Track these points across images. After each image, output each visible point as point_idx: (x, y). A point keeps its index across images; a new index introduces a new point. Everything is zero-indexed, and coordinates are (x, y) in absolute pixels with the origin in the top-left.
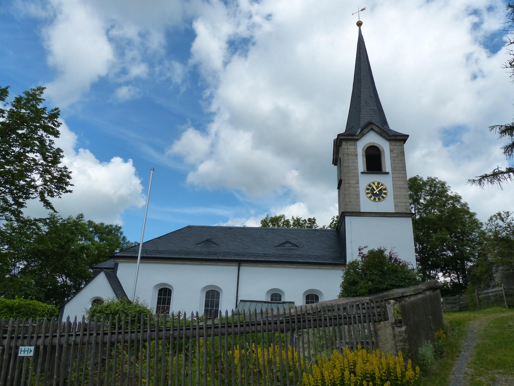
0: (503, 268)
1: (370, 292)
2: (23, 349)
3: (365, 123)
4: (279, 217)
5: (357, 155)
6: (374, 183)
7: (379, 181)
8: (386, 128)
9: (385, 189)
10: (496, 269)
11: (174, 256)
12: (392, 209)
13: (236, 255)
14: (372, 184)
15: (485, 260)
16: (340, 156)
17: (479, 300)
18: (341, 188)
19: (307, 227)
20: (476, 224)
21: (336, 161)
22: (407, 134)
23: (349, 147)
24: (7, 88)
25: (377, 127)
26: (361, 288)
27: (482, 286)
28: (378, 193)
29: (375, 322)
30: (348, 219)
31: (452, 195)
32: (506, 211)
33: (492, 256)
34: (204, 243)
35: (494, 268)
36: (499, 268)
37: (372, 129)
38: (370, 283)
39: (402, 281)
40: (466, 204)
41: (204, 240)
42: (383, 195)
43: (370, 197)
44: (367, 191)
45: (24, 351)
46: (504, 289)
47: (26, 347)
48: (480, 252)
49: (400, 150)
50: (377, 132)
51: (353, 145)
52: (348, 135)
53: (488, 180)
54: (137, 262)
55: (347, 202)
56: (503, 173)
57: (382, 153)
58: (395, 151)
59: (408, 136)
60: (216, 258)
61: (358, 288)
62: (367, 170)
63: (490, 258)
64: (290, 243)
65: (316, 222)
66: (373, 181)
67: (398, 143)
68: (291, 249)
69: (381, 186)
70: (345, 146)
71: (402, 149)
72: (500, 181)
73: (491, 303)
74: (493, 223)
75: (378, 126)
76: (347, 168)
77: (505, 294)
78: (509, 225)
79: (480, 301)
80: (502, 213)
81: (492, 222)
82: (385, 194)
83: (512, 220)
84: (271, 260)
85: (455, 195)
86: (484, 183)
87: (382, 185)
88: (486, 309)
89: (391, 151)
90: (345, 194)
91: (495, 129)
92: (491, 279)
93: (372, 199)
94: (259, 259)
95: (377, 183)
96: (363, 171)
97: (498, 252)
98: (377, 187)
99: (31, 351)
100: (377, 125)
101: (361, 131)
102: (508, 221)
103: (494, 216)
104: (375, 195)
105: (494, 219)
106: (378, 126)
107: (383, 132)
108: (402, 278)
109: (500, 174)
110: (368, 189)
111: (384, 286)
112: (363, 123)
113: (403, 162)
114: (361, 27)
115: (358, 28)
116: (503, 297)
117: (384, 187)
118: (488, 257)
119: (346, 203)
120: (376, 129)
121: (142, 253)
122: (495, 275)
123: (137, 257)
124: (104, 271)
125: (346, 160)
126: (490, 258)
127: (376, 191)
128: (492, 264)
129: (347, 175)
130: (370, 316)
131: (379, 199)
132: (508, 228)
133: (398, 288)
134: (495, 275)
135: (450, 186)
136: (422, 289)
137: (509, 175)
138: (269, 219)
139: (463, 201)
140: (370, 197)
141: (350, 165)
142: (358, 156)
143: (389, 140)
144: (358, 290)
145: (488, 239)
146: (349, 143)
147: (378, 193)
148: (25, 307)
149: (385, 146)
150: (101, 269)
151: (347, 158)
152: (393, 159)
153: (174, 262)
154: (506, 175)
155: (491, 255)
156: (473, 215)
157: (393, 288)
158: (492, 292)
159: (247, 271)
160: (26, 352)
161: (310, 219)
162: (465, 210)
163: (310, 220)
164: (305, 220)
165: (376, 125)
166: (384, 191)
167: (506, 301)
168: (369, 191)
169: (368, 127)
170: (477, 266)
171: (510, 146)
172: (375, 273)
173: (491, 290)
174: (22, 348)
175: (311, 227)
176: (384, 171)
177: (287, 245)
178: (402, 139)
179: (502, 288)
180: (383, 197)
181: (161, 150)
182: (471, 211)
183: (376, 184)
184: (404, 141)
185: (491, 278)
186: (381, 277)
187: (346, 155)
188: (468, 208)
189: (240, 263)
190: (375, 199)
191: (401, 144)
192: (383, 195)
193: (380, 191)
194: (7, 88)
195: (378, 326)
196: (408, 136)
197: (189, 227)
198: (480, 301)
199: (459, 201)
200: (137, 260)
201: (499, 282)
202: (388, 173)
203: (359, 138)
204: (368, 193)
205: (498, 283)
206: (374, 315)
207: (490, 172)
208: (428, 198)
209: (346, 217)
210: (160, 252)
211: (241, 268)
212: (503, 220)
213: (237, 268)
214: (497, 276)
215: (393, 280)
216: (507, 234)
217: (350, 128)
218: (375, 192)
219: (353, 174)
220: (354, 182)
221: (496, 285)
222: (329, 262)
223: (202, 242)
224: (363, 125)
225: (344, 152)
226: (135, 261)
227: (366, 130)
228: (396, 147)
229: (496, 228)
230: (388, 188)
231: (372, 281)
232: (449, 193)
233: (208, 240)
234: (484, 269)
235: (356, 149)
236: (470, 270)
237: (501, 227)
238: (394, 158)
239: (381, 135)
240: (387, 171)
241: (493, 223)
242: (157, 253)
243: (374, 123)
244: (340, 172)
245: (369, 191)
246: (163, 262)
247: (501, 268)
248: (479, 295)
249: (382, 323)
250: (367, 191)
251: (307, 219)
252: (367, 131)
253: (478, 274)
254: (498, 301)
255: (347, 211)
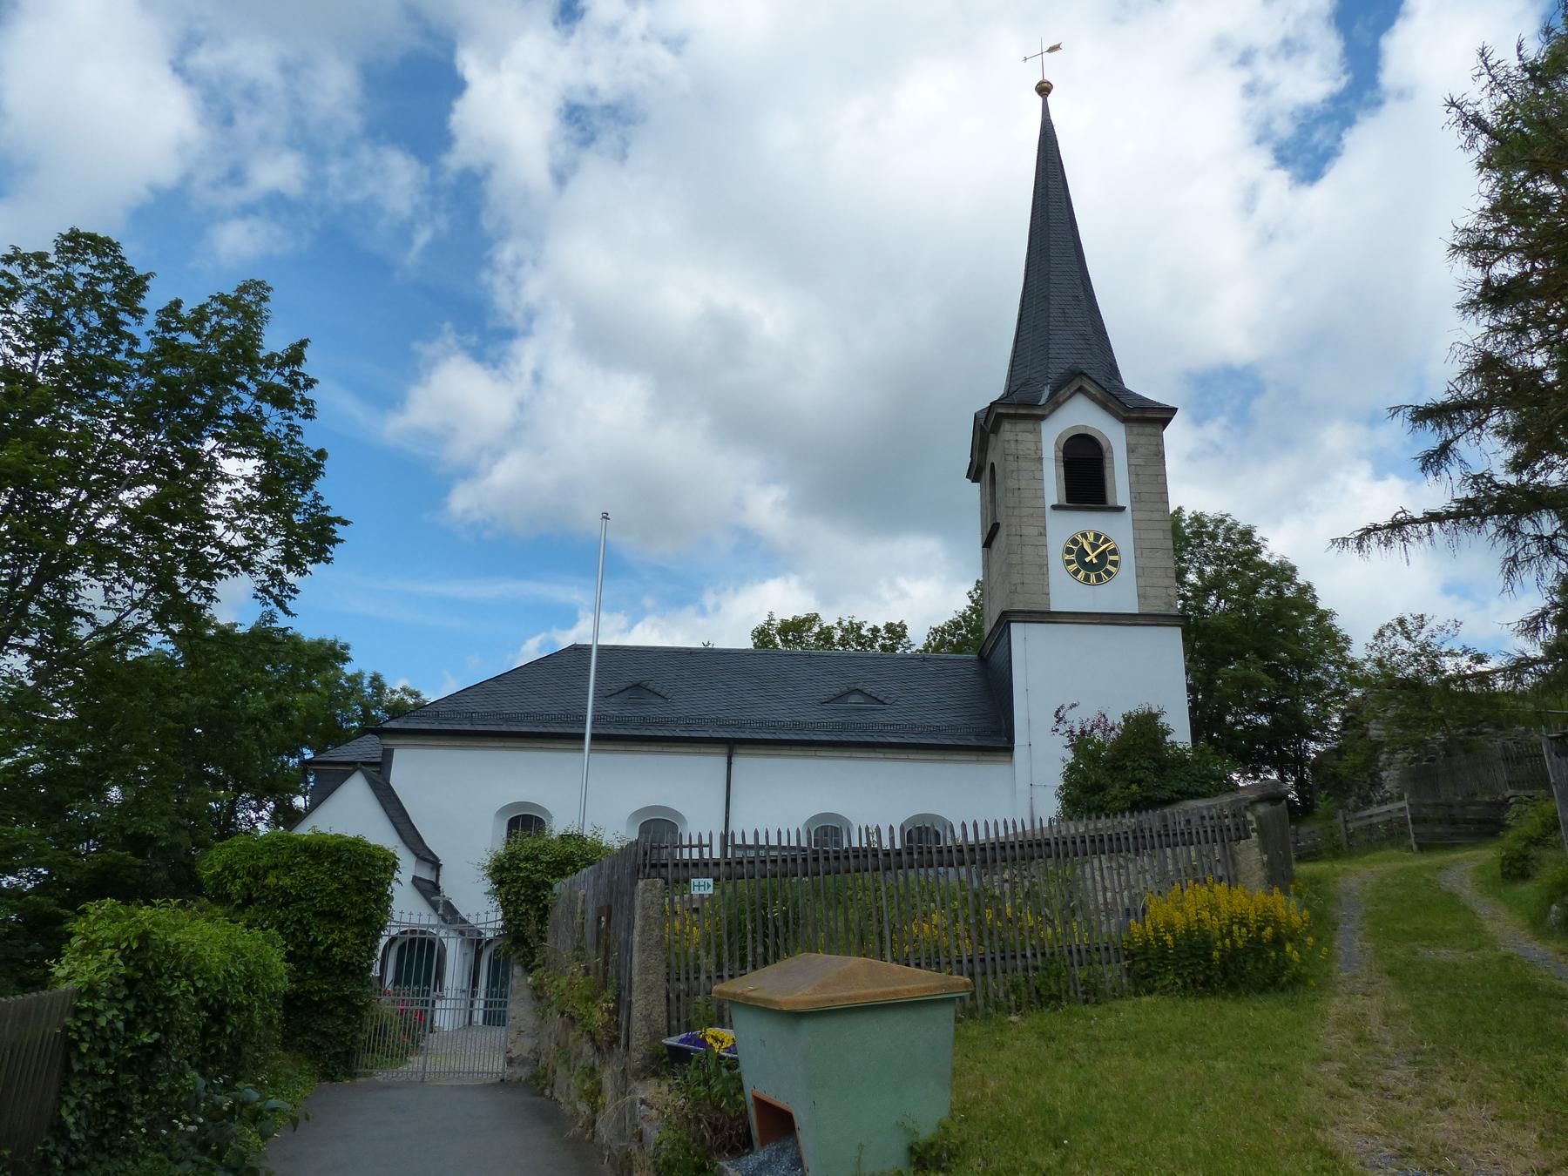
0: (1406, 755)
1: (1136, 807)
2: (696, 884)
3: (1062, 371)
4: (805, 620)
5: (1040, 459)
6: (1084, 536)
7: (1099, 529)
8: (1116, 387)
9: (1114, 552)
10: (1387, 759)
11: (552, 730)
12: (1129, 603)
13: (720, 726)
14: (1080, 538)
15: (1364, 735)
16: (993, 457)
17: (1347, 835)
18: (996, 544)
19: (883, 647)
20: (1332, 639)
21: (975, 473)
22: (1171, 404)
23: (1019, 438)
24: (147, 278)
25: (1094, 385)
26: (1115, 798)
27: (1351, 801)
28: (1095, 561)
29: (1231, 840)
30: (1017, 630)
31: (1272, 561)
32: (1417, 613)
33: (1381, 727)
34: (627, 693)
35: (1383, 757)
36: (1396, 756)
37: (1081, 390)
38: (1134, 787)
39: (1203, 783)
40: (1310, 586)
41: (623, 686)
42: (1109, 567)
43: (1076, 572)
44: (1067, 557)
45: (699, 886)
46: (1410, 805)
47: (700, 880)
48: (1347, 715)
49: (1153, 448)
50: (1093, 398)
51: (1031, 432)
52: (1019, 405)
53: (1379, 539)
54: (583, 750)
55: (1015, 584)
56: (1414, 521)
57: (1107, 455)
58: (1141, 450)
59: (1173, 411)
60: (667, 734)
61: (1108, 798)
62: (1068, 500)
63: (1375, 731)
64: (861, 692)
65: (908, 632)
66: (1082, 529)
67: (1149, 429)
68: (866, 710)
69: (1103, 543)
70: (1008, 431)
71: (1157, 445)
72: (1408, 541)
73: (1377, 840)
74: (1386, 645)
75: (1095, 382)
76: (1016, 493)
77: (1412, 819)
78: (1423, 649)
79: (1350, 836)
80: (1409, 619)
81: (1383, 641)
82: (1115, 564)
83: (1432, 636)
84: (815, 738)
85: (1281, 562)
86: (1368, 546)
87: (1106, 541)
88: (1367, 854)
89: (1131, 450)
90: (1010, 565)
91: (1401, 413)
92: (1373, 785)
93: (1079, 577)
94: (784, 737)
95: (1092, 534)
96: (1056, 503)
97: (1397, 715)
98: (1094, 547)
99: (709, 886)
100: (1094, 376)
101: (1053, 394)
102: (1422, 637)
103: (1389, 625)
104: (1089, 567)
105: (1388, 633)
106: (1095, 382)
107: (1111, 397)
108: (1202, 778)
109: (1407, 523)
110: (1069, 551)
111: (1166, 794)
112: (1056, 370)
113: (1160, 479)
114: (1049, 98)
115: (1040, 99)
116: (1406, 824)
117: (1112, 547)
118: (1368, 729)
119: (1014, 588)
120: (1093, 391)
121: (593, 727)
122: (1384, 774)
123: (581, 737)
124: (364, 772)
125: (1013, 471)
126: (1375, 731)
127: (1092, 557)
128: (1377, 746)
129: (1016, 512)
130: (1221, 830)
131: (1099, 578)
132: (1420, 655)
133: (1193, 799)
134: (1384, 774)
135: (1264, 536)
136: (1247, 799)
137: (1430, 532)
138: (777, 622)
139: (1301, 579)
140: (1076, 572)
141: (1023, 484)
142: (1045, 463)
143: (1125, 420)
144: (1108, 803)
145: (1364, 682)
146: (1021, 426)
147: (1095, 561)
148: (349, 850)
149: (1114, 435)
150: (351, 767)
151: (1013, 465)
152: (1134, 471)
153: (551, 746)
154: (1423, 528)
155: (1377, 723)
156: (1324, 615)
157: (1183, 799)
158: (1378, 815)
159: (749, 767)
160: (702, 888)
161: (892, 624)
162: (1305, 601)
163: (890, 628)
164: (875, 630)
165: (1090, 378)
166: (1111, 558)
167: (1413, 835)
168: (1072, 557)
169: (1070, 383)
170: (1339, 752)
171: (1435, 452)
172: (1145, 765)
173: (1375, 810)
174: (694, 881)
175: (893, 649)
176: (1110, 502)
177: (854, 699)
178: (1160, 416)
179: (1404, 804)
180: (1109, 573)
181: (390, 401)
182: (1322, 605)
183: (1091, 539)
184: (1165, 422)
185: (1376, 783)
186: (1156, 776)
187: (1011, 458)
188: (1314, 597)
189: (732, 746)
190: (1087, 578)
191: (1154, 430)
192: (1109, 567)
193: (1102, 556)
194: (147, 278)
195: (1237, 848)
196: (1173, 411)
197: (576, 649)
198: (1350, 836)
199: (1291, 579)
200: (584, 744)
201: (1395, 791)
202: (1122, 509)
203: (1046, 412)
204: (1069, 562)
205: (1392, 794)
206: (1229, 830)
207: (1384, 519)
208: (1209, 570)
209: (1013, 625)
210: (508, 719)
211: (735, 760)
212: (1409, 638)
213: (724, 759)
214: (1390, 778)
215: (1182, 780)
216: (1418, 671)
217: (1019, 382)
218: (1087, 560)
219: (1030, 511)
220: (1033, 531)
221: (1388, 799)
222: (969, 743)
223: (622, 691)
224: (1055, 376)
225: (1007, 452)
226: (577, 747)
227: (1064, 392)
228: (1143, 440)
229: (1392, 655)
230: (1121, 549)
231: (1139, 782)
232: (1264, 557)
233: (638, 685)
234: (1359, 760)
235: (1038, 442)
236: (1316, 766)
237: (1403, 653)
238: (1138, 468)
239: (1105, 406)
240: (1120, 504)
241: (1386, 645)
242: (500, 722)
243: (1085, 371)
244: (991, 502)
245: (1072, 557)
246: (442, 743)
247: (1400, 756)
248: (1346, 822)
249: (1242, 842)
250: (1067, 557)
251: (881, 627)
252: (1068, 394)
253: (1345, 772)
254: (1393, 835)
255: (1016, 608)
